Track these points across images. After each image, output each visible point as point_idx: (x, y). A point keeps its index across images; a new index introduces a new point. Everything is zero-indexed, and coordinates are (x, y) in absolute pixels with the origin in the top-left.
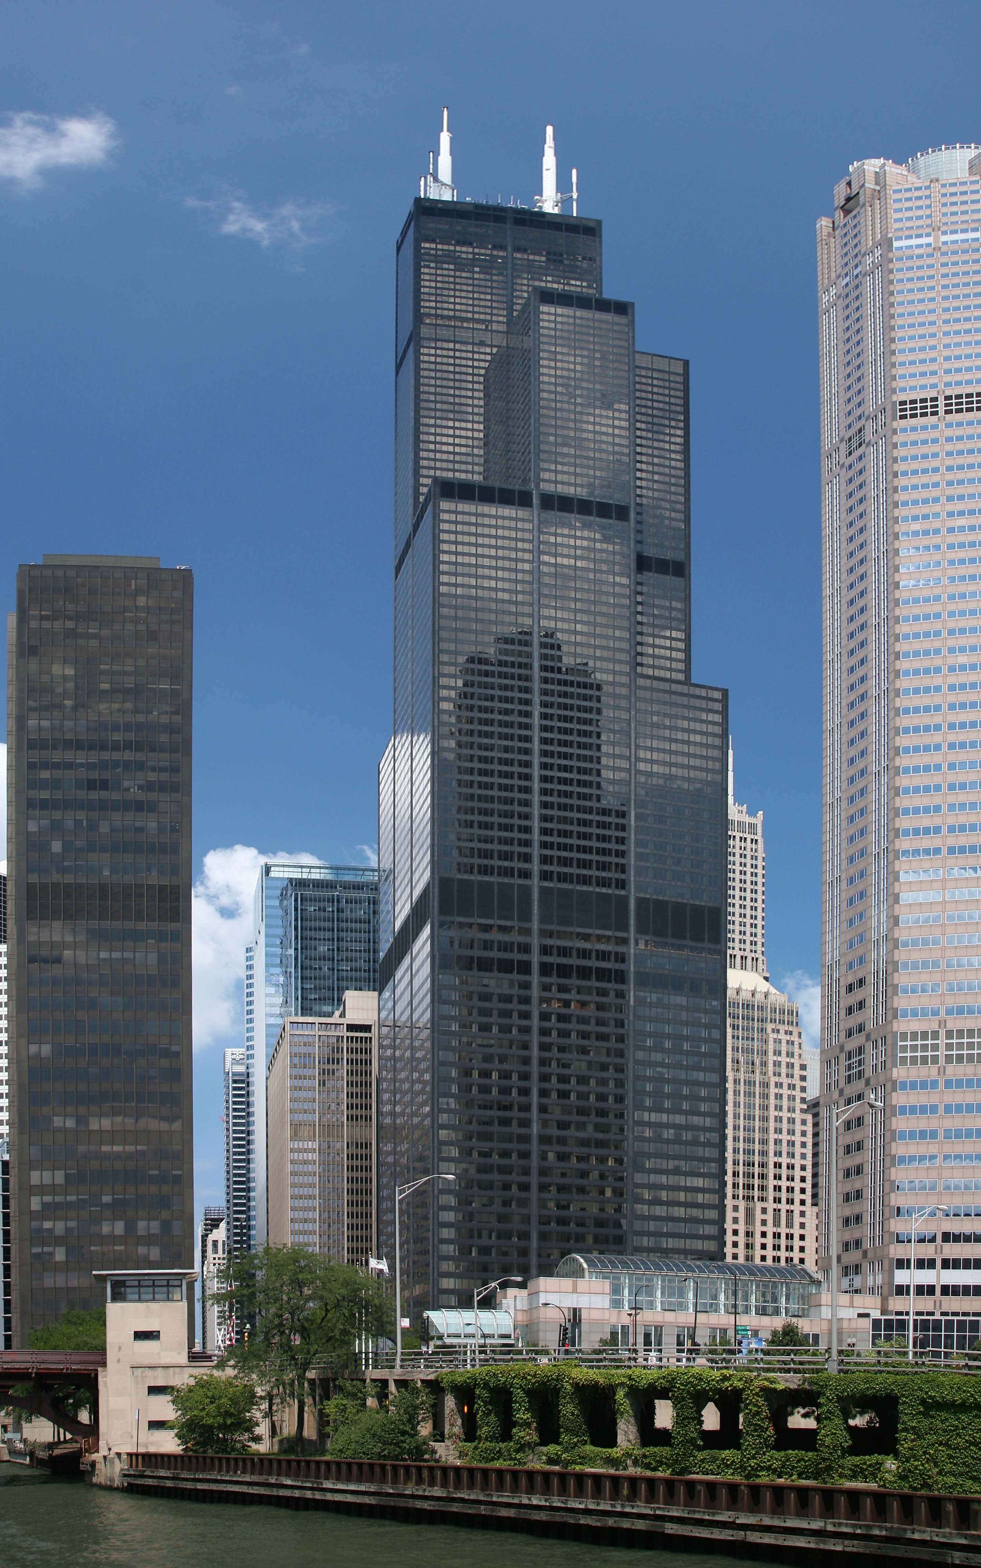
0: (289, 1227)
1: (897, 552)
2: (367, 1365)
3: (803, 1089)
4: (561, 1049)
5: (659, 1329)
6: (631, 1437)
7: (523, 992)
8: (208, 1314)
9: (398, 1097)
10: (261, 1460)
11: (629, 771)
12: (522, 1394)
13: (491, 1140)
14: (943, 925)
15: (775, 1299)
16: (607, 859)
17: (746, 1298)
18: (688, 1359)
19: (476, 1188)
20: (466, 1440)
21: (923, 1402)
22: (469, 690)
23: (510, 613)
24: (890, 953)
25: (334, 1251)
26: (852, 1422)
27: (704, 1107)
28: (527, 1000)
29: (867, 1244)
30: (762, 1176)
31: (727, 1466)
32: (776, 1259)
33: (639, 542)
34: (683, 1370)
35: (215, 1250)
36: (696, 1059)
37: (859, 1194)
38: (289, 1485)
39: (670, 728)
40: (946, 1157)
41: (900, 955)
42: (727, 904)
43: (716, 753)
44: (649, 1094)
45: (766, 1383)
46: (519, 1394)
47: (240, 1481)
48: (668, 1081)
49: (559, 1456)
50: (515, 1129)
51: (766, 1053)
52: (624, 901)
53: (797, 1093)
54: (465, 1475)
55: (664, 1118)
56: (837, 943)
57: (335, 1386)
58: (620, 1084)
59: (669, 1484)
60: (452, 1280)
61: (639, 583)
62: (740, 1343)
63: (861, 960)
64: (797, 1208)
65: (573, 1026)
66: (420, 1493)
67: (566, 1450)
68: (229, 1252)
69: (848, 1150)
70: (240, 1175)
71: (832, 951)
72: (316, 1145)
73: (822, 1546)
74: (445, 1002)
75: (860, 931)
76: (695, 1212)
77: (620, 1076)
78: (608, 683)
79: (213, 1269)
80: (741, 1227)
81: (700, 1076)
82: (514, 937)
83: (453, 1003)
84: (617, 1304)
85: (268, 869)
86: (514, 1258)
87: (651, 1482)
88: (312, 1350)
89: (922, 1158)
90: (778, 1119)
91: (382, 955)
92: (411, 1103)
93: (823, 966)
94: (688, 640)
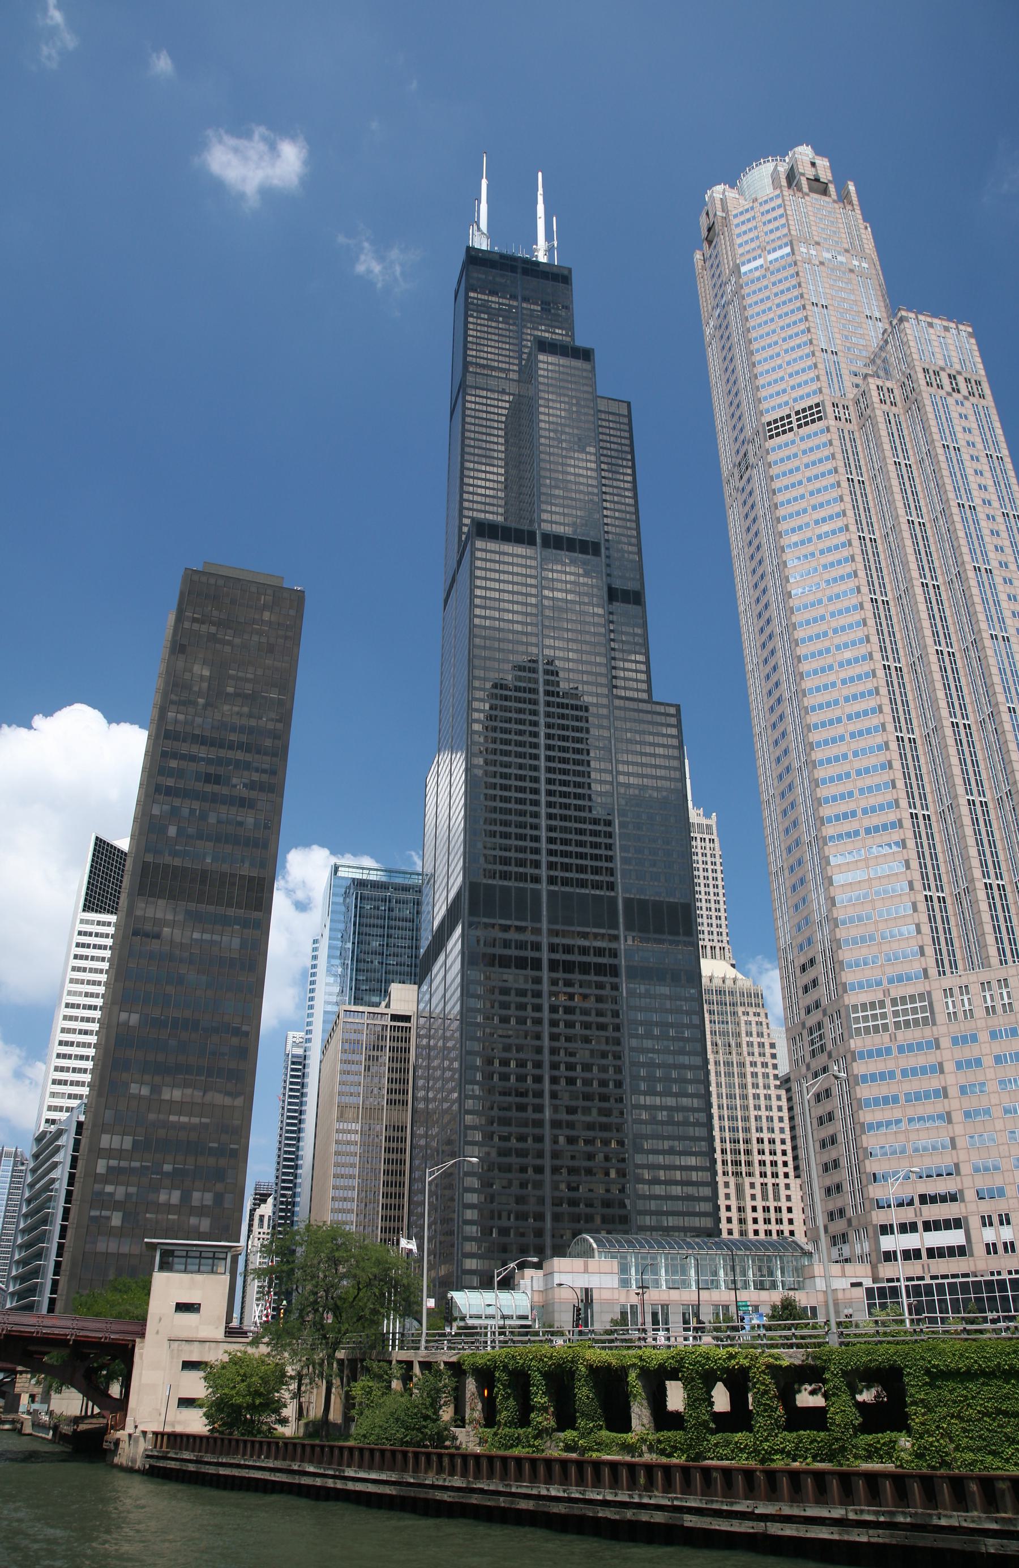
0: (330, 1205)
1: (785, 563)
2: (393, 1346)
3: (775, 1067)
4: (568, 1039)
5: (665, 1307)
6: (645, 1421)
7: (536, 987)
8: (248, 1288)
9: (431, 1083)
10: (286, 1444)
11: (611, 783)
12: (539, 1377)
13: (510, 1125)
14: (872, 901)
15: (771, 1273)
16: (599, 864)
17: (744, 1274)
18: (695, 1338)
19: (496, 1171)
20: (486, 1426)
21: (928, 1372)
22: (494, 713)
23: (522, 643)
24: (832, 931)
25: (369, 1230)
26: (860, 1398)
27: (691, 1089)
28: (538, 994)
29: (850, 1213)
30: (748, 1152)
31: (742, 1450)
32: (769, 1233)
33: (609, 575)
34: (690, 1349)
35: (261, 1226)
36: (681, 1044)
37: (836, 1164)
38: (312, 1472)
39: (641, 743)
40: (911, 1120)
41: (841, 933)
42: (695, 900)
43: (675, 763)
44: (643, 1079)
45: (771, 1360)
46: (536, 1377)
47: (262, 1467)
48: (659, 1066)
49: (576, 1443)
50: (530, 1114)
51: (739, 1035)
52: (613, 901)
53: (770, 1070)
54: (484, 1463)
55: (658, 1101)
56: (787, 927)
57: (362, 1366)
58: (618, 1070)
59: (685, 1470)
60: (474, 1261)
61: (611, 613)
62: (742, 1319)
63: (810, 941)
64: (781, 1181)
65: (577, 1017)
66: (440, 1483)
67: (582, 1436)
68: (274, 1228)
69: (821, 1121)
70: (289, 1153)
71: (784, 937)
72: (358, 1127)
73: (846, 1537)
74: (473, 996)
75: (805, 914)
76: (691, 1190)
77: (618, 1063)
78: (593, 704)
79: (258, 1244)
80: (733, 1203)
81: (685, 1060)
82: (528, 937)
83: (478, 997)
84: (625, 1283)
85: (336, 869)
86: (531, 1239)
87: (667, 1469)
88: (343, 1329)
89: (889, 1123)
90: (756, 1097)
91: (422, 951)
92: (442, 1089)
93: (779, 950)
94: (647, 663)
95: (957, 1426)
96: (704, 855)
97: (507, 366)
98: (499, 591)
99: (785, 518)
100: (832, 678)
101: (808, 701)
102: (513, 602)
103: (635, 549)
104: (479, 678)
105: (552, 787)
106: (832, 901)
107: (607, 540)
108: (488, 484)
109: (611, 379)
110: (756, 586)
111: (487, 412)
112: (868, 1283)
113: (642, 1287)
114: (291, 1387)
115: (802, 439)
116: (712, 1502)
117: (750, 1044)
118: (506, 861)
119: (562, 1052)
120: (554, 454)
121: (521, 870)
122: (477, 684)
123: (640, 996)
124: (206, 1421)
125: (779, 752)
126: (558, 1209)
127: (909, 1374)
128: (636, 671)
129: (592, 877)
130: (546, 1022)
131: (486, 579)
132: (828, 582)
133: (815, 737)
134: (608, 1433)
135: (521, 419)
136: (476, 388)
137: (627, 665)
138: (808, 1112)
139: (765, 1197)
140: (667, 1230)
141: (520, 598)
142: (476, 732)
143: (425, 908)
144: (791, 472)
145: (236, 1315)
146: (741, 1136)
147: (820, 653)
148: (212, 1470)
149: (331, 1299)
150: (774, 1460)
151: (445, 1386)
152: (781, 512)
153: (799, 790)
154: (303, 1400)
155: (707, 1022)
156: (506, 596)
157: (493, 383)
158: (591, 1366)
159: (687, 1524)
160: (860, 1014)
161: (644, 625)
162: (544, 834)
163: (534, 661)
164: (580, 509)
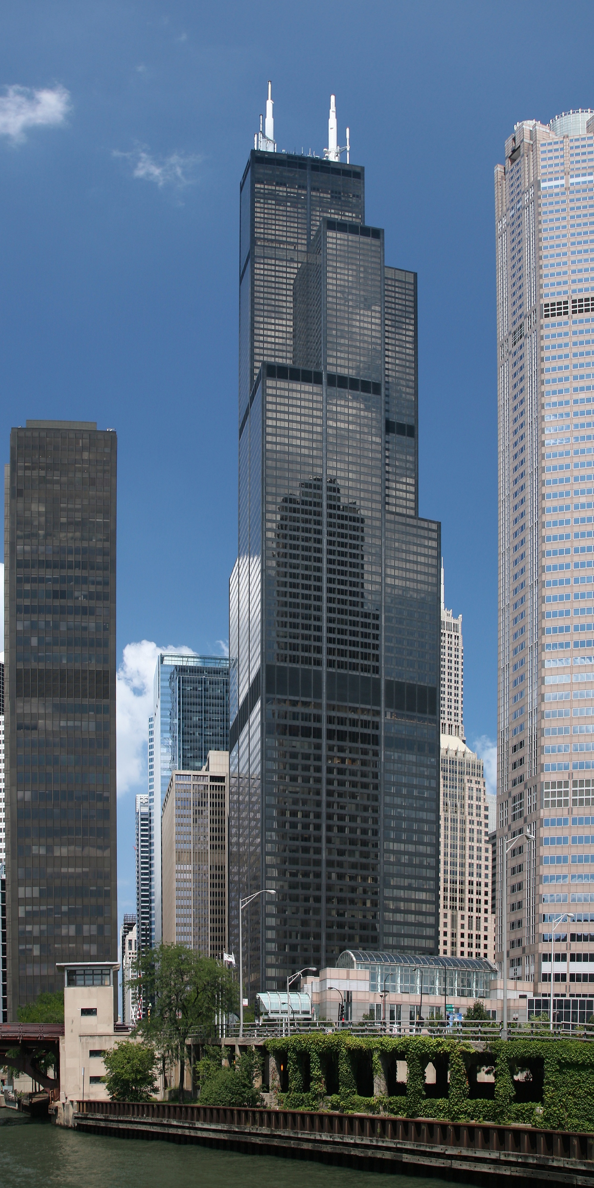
0: (175, 929)
1: (543, 417)
2: (222, 1034)
3: (486, 825)
4: (340, 795)
5: (399, 1006)
6: (382, 1089)
7: (317, 752)
8: (126, 995)
9: (241, 831)
10: (158, 1106)
11: (380, 584)
13: (297, 864)
15: (469, 985)
16: (367, 651)
18: (417, 1030)
19: (288, 901)
20: (282, 1091)
21: (559, 1062)
22: (284, 523)
23: (309, 465)
24: (539, 721)
26: (516, 1078)
27: (426, 839)
28: (318, 758)
29: (525, 943)
30: (462, 891)
31: (441, 1111)
32: (470, 954)
33: (387, 411)
34: (413, 1038)
35: (130, 948)
36: (422, 802)
38: (176, 1125)
41: (545, 724)
42: (440, 685)
43: (433, 571)
44: (393, 829)
45: (464, 1048)
46: (314, 1056)
47: (145, 1123)
48: (404, 819)
49: (339, 1103)
50: (312, 855)
51: (463, 798)
52: (377, 682)
53: (483, 828)
54: (281, 1117)
55: (402, 847)
56: (507, 714)
58: (375, 821)
59: (405, 1123)
60: (274, 970)
61: (387, 442)
62: (448, 1017)
63: (522, 727)
64: (482, 915)
65: (347, 777)
66: (254, 1131)
67: (343, 1099)
68: (139, 949)
71: (504, 722)
77: (376, 815)
79: (129, 961)
81: (424, 815)
82: (311, 710)
83: (274, 760)
84: (373, 988)
85: (162, 658)
86: (311, 953)
87: (394, 1122)
88: (189, 1023)
89: (559, 877)
91: (231, 723)
92: (249, 836)
93: (498, 732)
94: (416, 486)
95: (571, 1100)
96: (450, 648)
97: (296, 241)
98: (289, 421)
99: (548, 382)
100: (568, 516)
101: (545, 532)
102: (301, 431)
103: (412, 391)
104: (272, 494)
105: (332, 586)
106: (542, 697)
107: (387, 382)
108: (277, 334)
109: (397, 253)
110: (515, 432)
111: (275, 277)
112: (530, 996)
113: (385, 991)
114: (159, 1066)
115: (574, 322)
116: (420, 1145)
117: (471, 806)
118: (294, 647)
119: (335, 806)
120: (340, 311)
121: (306, 654)
122: (269, 498)
123: (394, 762)
124: (108, 1092)
125: (517, 570)
126: (330, 930)
127: (548, 1063)
128: (406, 492)
129: (362, 662)
130: (324, 781)
131: (276, 411)
132: (577, 439)
133: (547, 561)
134: (359, 1097)
135: (309, 286)
136: (264, 258)
137: (399, 486)
138: (506, 863)
139: (470, 927)
140: (403, 948)
141: (307, 427)
142: (270, 539)
143: (232, 688)
144: (560, 346)
145: (120, 1015)
146: (458, 878)
147: (561, 494)
148: (114, 1125)
149: (180, 1000)
150: (459, 1118)
151: (256, 1063)
152: (546, 376)
153: (529, 603)
154: (166, 1074)
155: (441, 786)
156: (295, 426)
157: (280, 254)
158: (349, 1048)
159: (404, 1160)
160: (550, 790)
161: (416, 454)
162: (324, 625)
163: (319, 480)
164: (364, 356)
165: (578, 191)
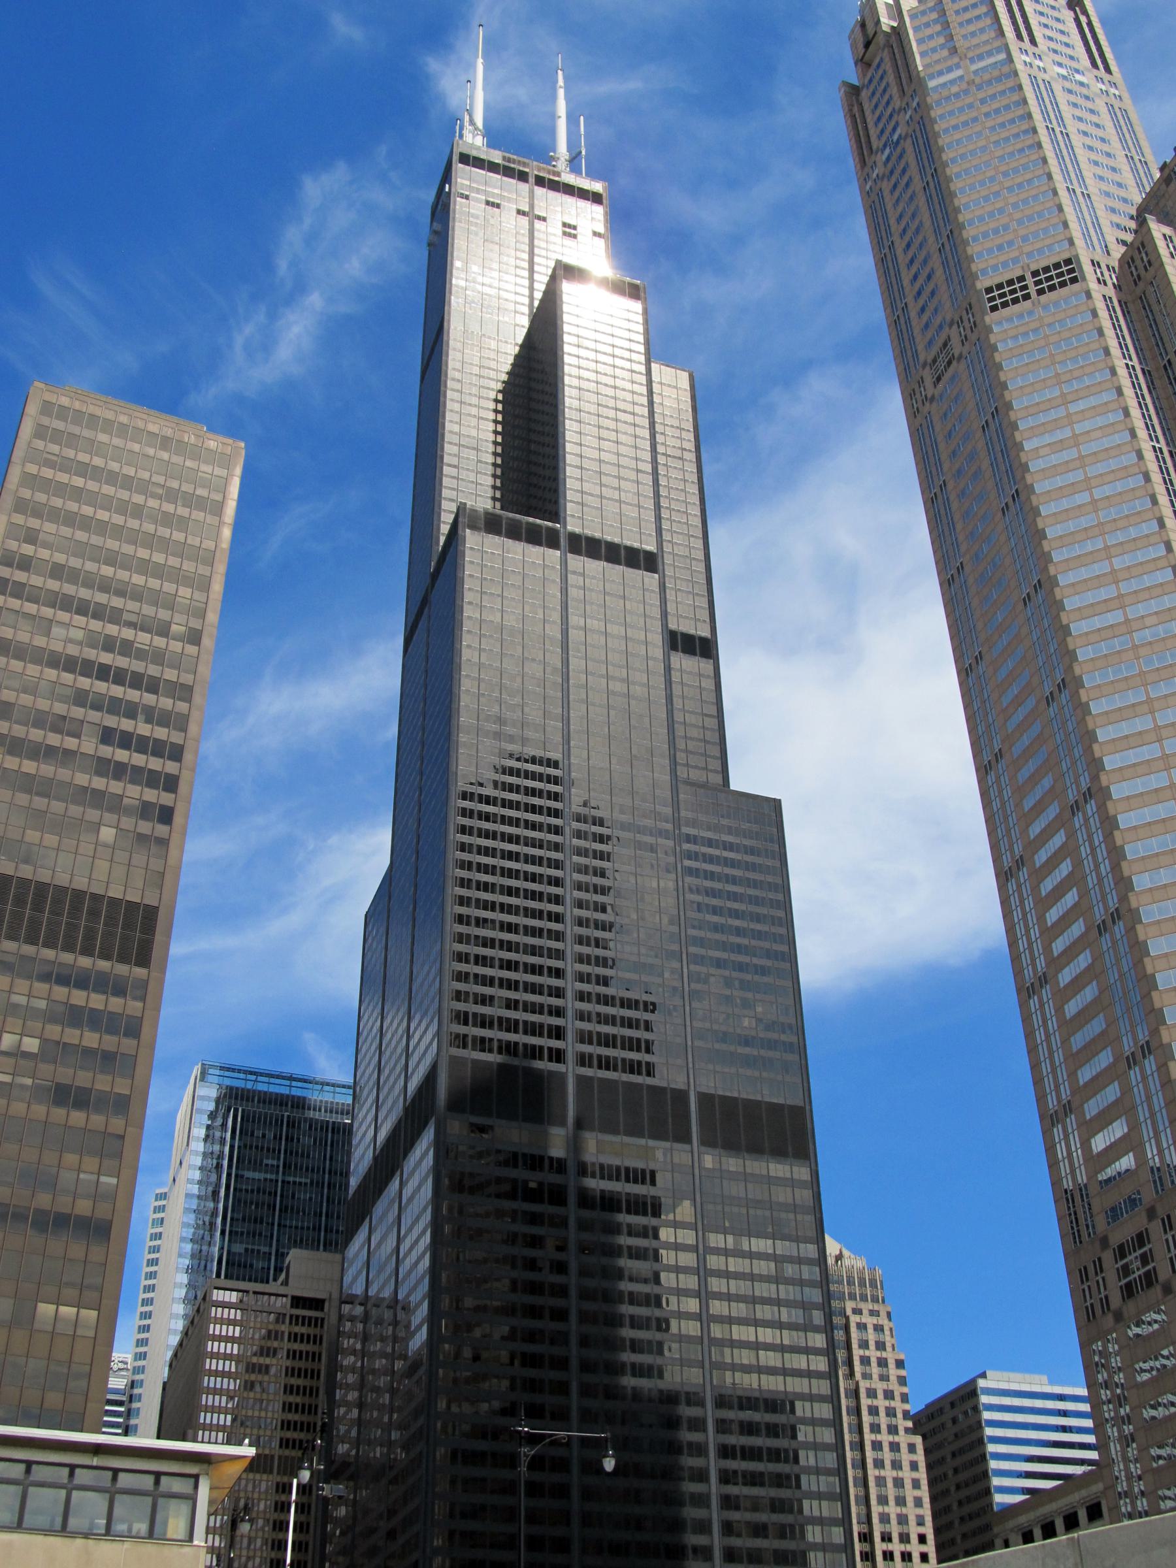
9: (354, 1433)
53: (897, 1404)
165: (989, 83)
